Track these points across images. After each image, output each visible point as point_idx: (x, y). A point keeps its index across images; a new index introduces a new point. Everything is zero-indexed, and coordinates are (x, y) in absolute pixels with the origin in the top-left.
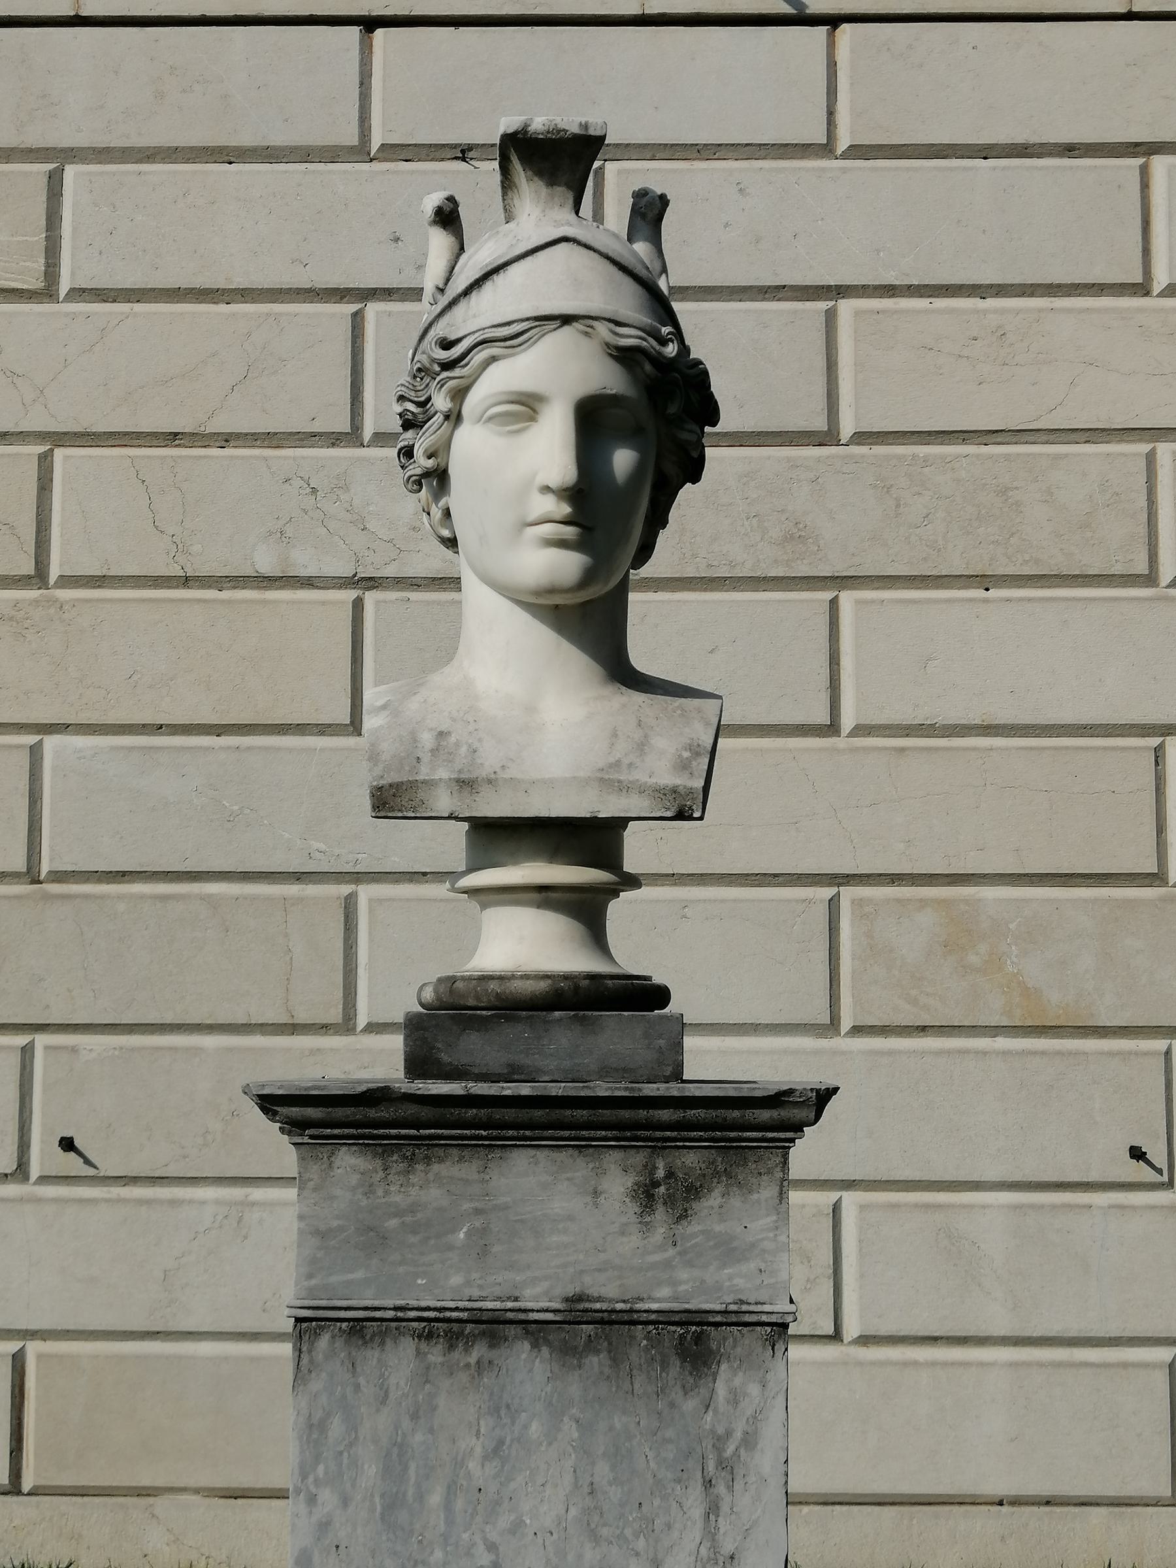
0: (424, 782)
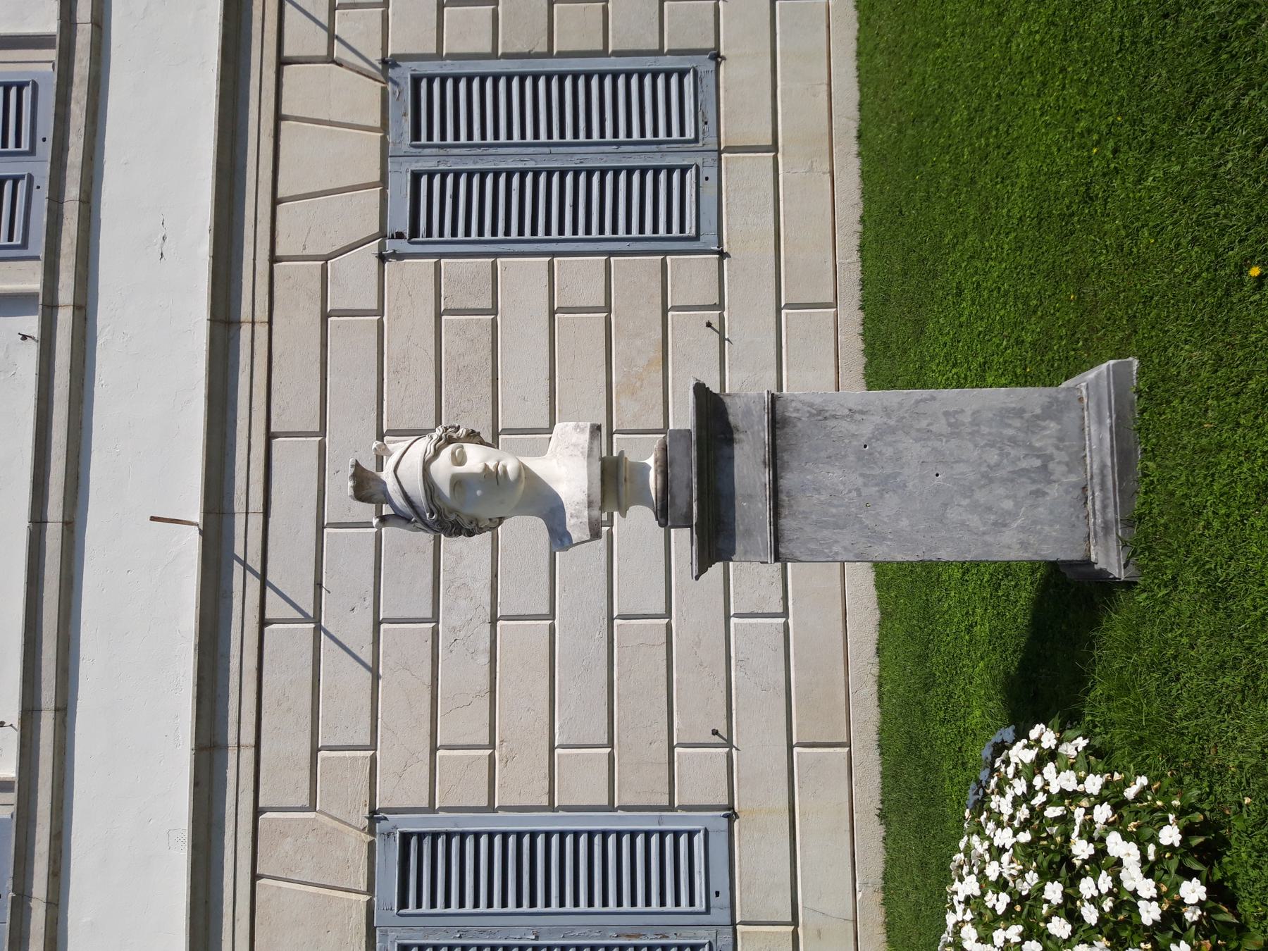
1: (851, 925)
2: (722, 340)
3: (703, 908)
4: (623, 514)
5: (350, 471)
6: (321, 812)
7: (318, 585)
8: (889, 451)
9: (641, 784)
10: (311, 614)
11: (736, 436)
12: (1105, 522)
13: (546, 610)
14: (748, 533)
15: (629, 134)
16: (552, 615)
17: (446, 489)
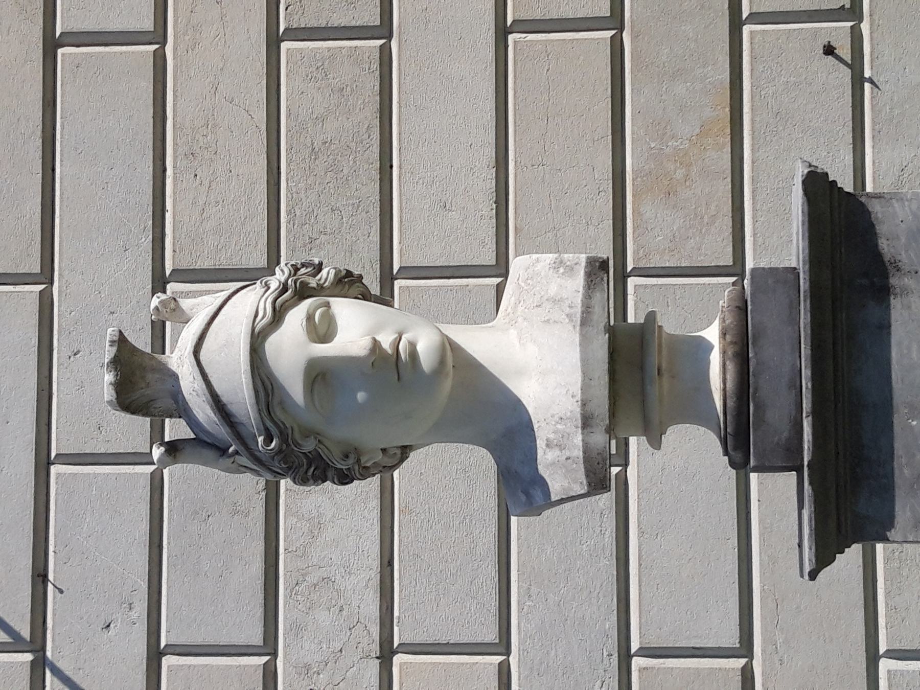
0: (584, 452)
2: (858, 81)
4: (656, 443)
5: (109, 353)
7: (40, 577)
10: (26, 633)
11: (893, 281)
13: (491, 635)
16: (504, 646)
17: (296, 389)
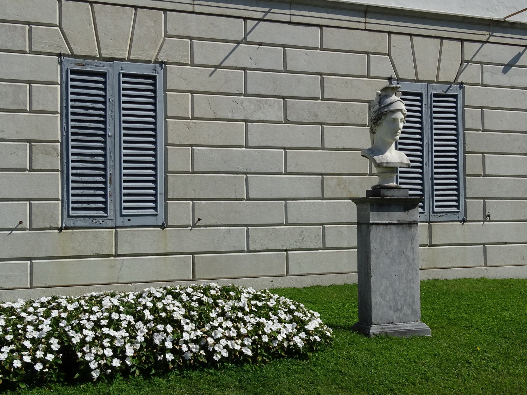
1: (116, 281)
3: (123, 213)
6: (164, 40)
7: (261, 44)
8: (402, 260)
9: (177, 185)
12: (384, 328)
14: (379, 215)
15: (436, 184)
17: (393, 116)
